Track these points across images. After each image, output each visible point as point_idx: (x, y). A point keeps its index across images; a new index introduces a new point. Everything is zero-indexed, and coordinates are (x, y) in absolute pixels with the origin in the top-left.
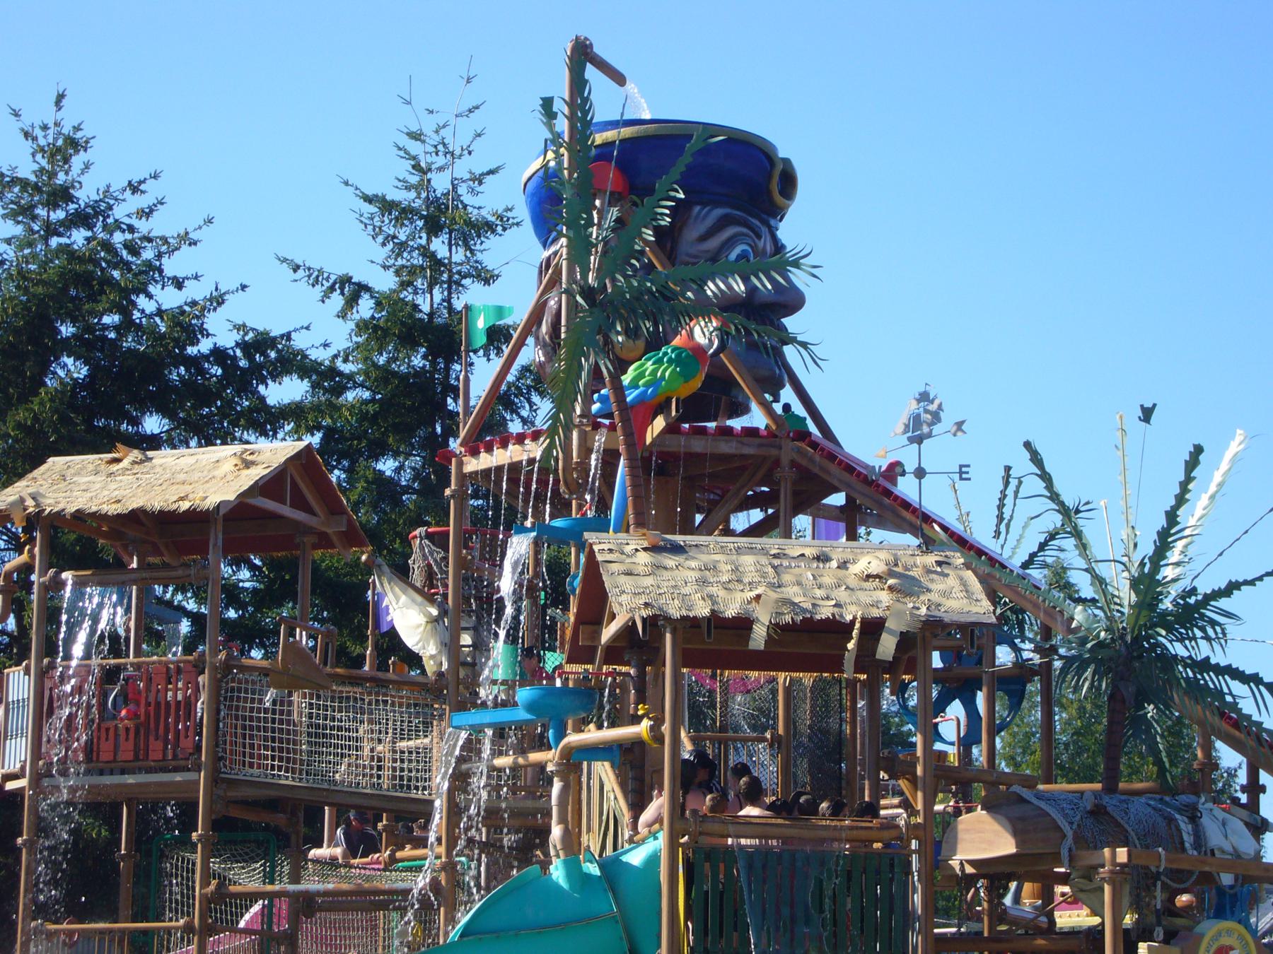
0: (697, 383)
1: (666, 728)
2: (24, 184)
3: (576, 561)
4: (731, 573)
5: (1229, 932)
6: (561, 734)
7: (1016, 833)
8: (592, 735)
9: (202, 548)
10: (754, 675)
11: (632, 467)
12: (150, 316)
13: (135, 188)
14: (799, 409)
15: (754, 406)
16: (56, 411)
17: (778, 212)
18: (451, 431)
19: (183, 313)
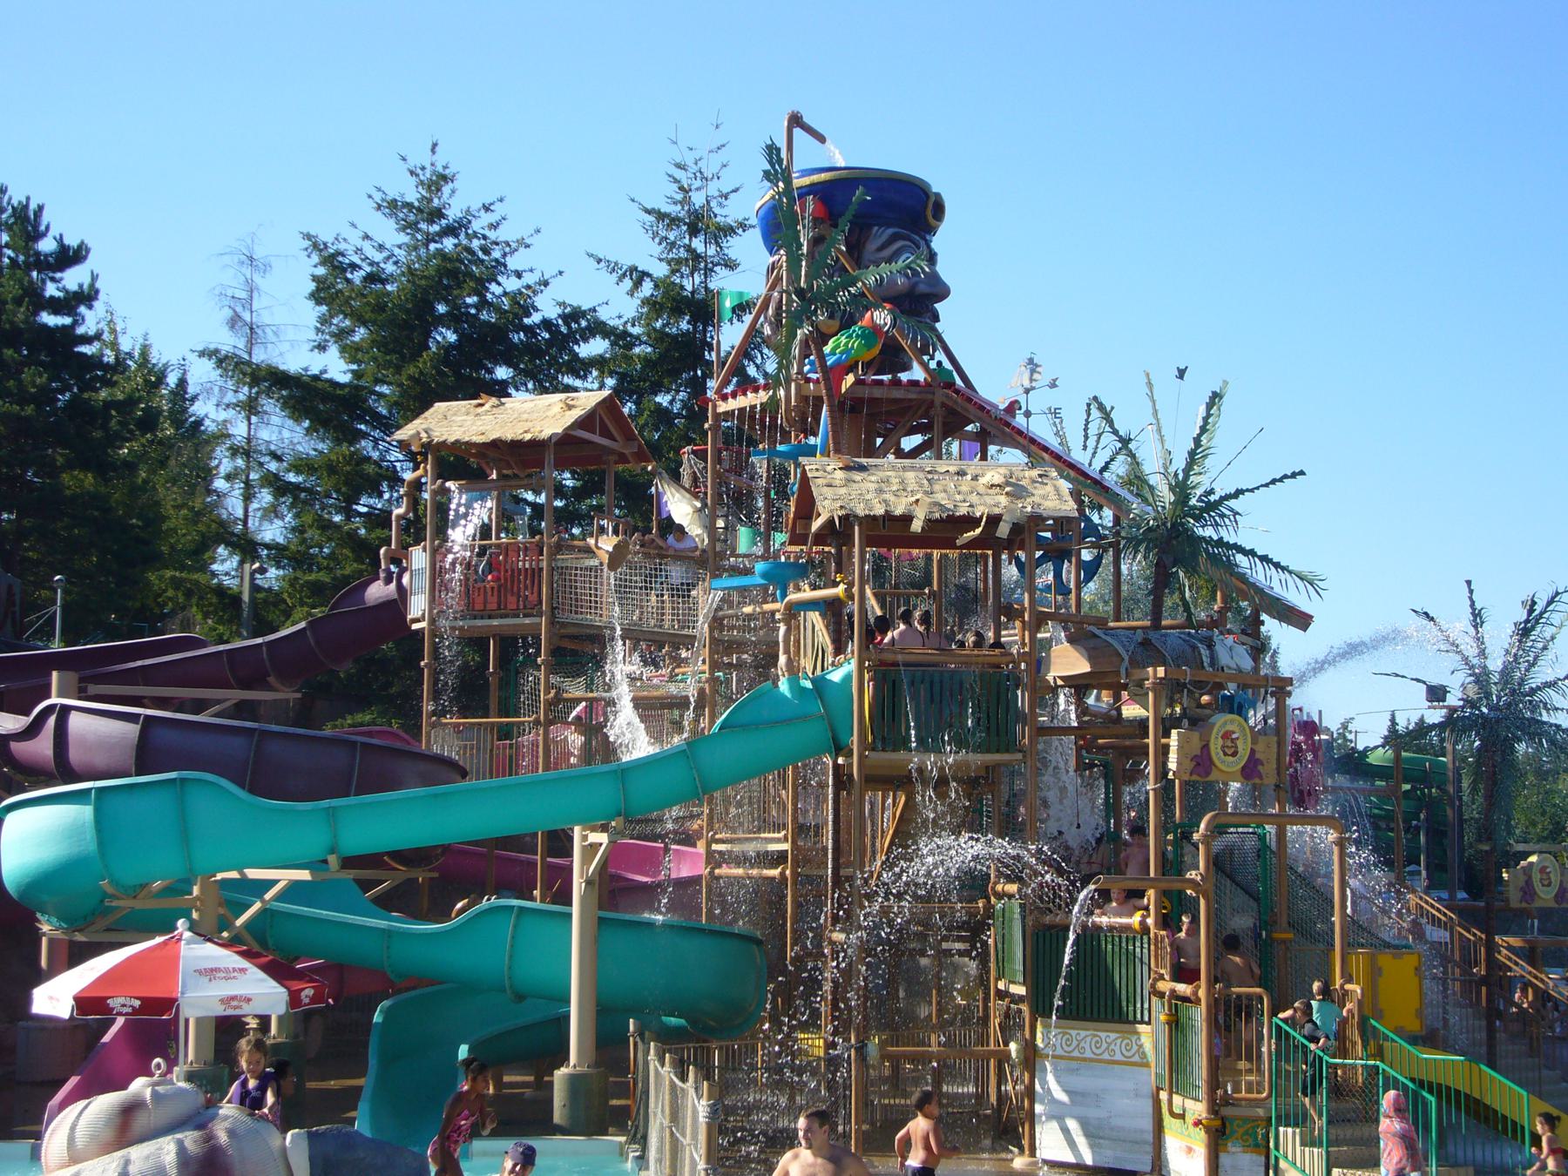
0: (876, 351)
1: (855, 590)
2: (409, 205)
3: (794, 480)
4: (899, 485)
5: (1232, 722)
6: (784, 595)
7: (1091, 659)
8: (807, 594)
9: (540, 464)
10: (915, 552)
11: (831, 411)
12: (498, 297)
13: (487, 208)
14: (947, 365)
15: (915, 365)
16: (433, 367)
17: (932, 230)
18: (708, 375)
19: (521, 293)
